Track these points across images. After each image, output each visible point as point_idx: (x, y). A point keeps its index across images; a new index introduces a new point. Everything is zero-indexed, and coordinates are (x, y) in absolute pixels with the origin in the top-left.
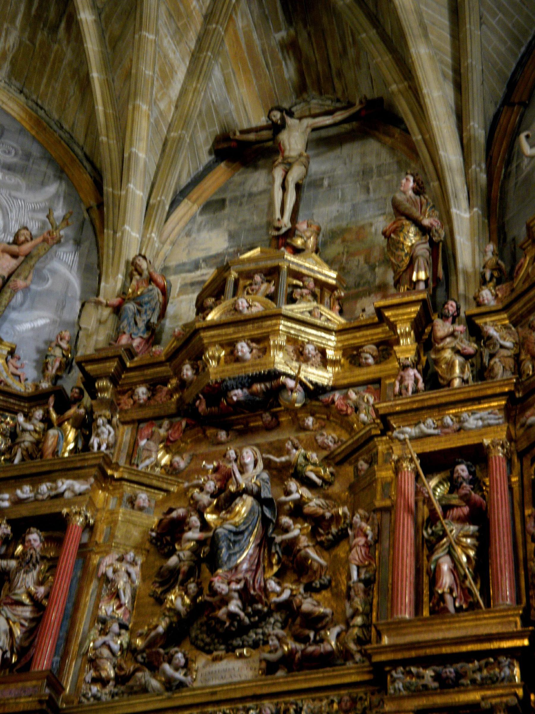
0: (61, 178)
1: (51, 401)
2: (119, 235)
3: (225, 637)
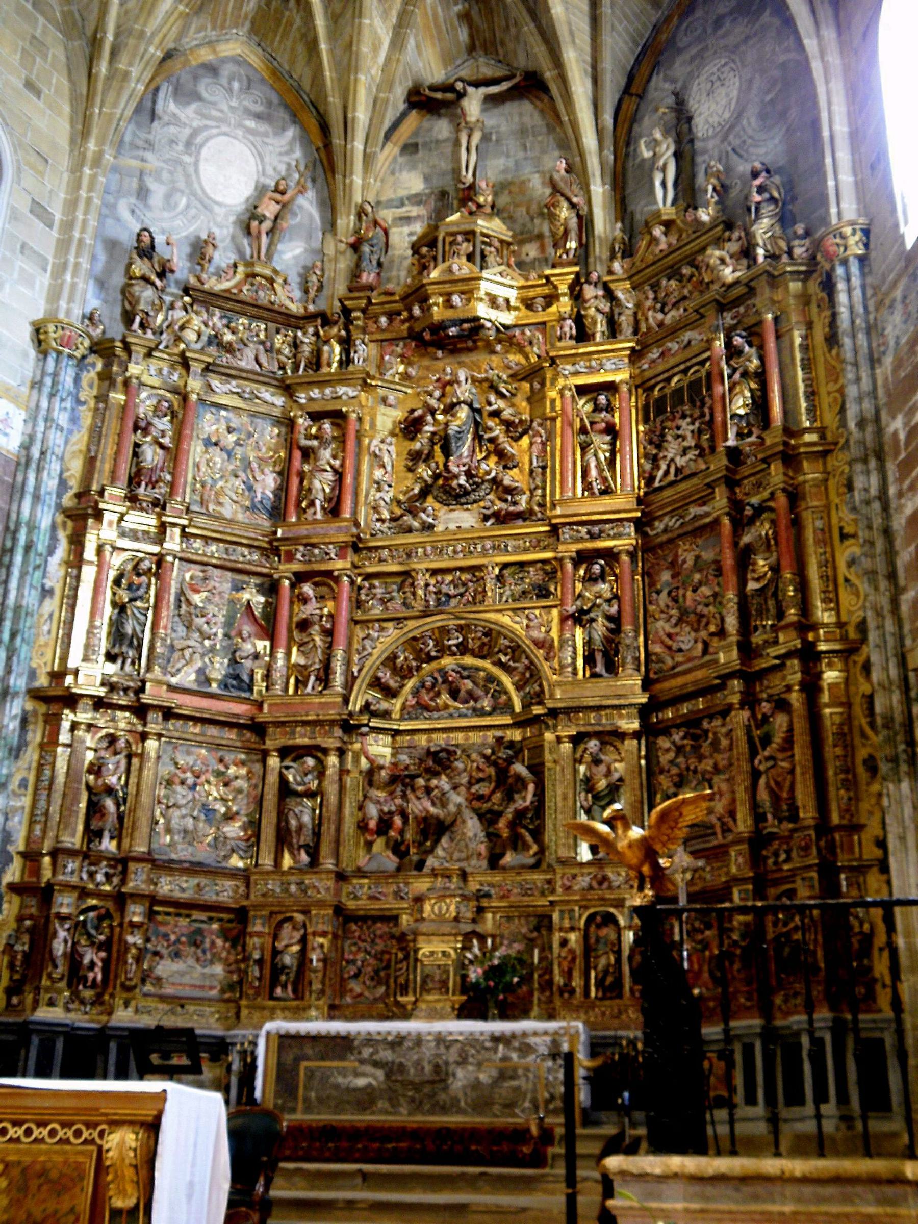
0: (295, 122)
1: (319, 321)
3: (455, 497)
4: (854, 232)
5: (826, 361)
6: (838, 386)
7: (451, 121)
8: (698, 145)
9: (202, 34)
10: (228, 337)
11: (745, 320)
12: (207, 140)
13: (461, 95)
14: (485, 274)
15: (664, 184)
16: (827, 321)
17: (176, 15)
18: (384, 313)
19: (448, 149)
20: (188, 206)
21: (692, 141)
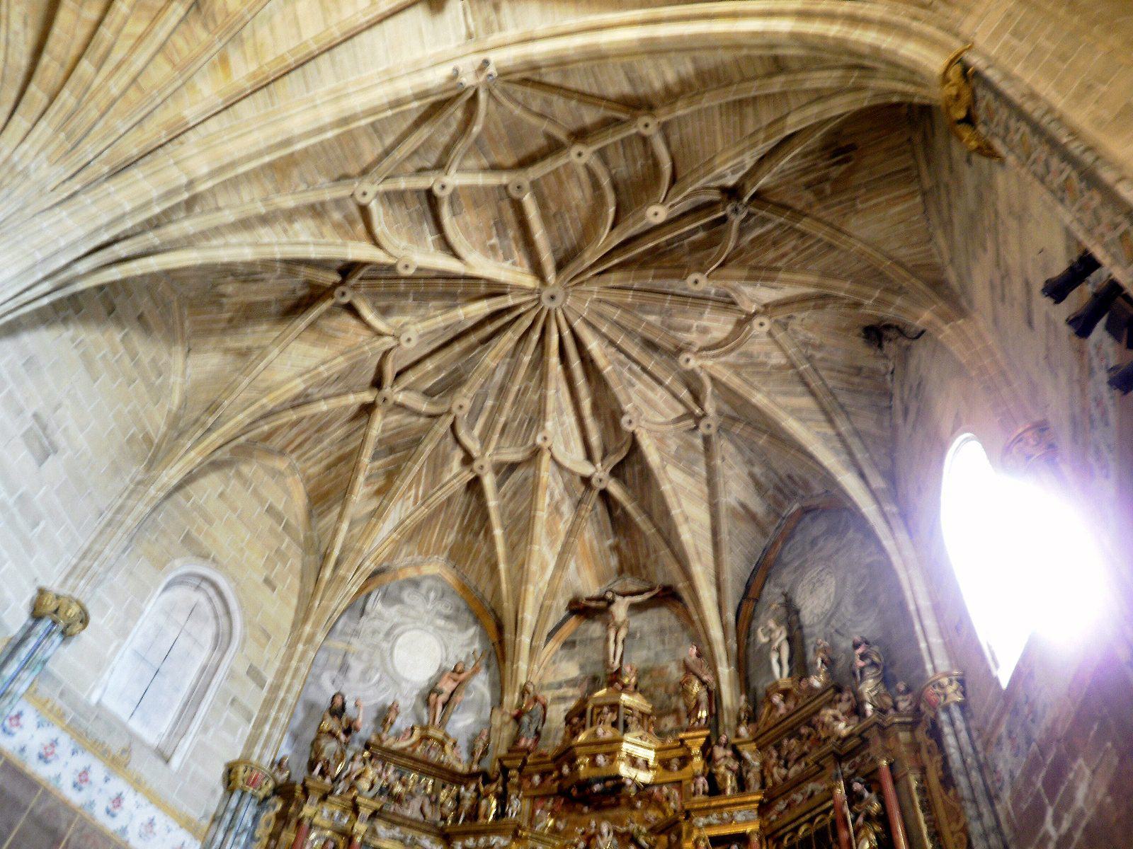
2: (515, 666)
4: (951, 682)
5: (944, 802)
6: (961, 824)
7: (603, 624)
8: (806, 631)
9: (410, 558)
10: (398, 789)
11: (863, 769)
12: (402, 633)
13: (611, 602)
14: (628, 737)
15: (780, 662)
16: (939, 765)
17: (390, 540)
18: (537, 772)
19: (600, 645)
20: (380, 680)
21: (801, 628)
